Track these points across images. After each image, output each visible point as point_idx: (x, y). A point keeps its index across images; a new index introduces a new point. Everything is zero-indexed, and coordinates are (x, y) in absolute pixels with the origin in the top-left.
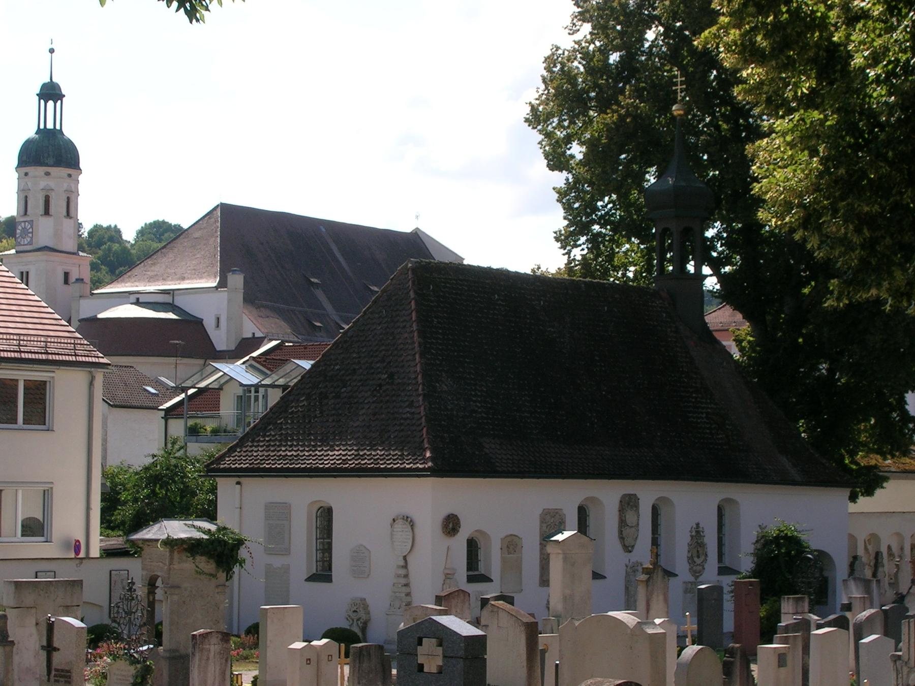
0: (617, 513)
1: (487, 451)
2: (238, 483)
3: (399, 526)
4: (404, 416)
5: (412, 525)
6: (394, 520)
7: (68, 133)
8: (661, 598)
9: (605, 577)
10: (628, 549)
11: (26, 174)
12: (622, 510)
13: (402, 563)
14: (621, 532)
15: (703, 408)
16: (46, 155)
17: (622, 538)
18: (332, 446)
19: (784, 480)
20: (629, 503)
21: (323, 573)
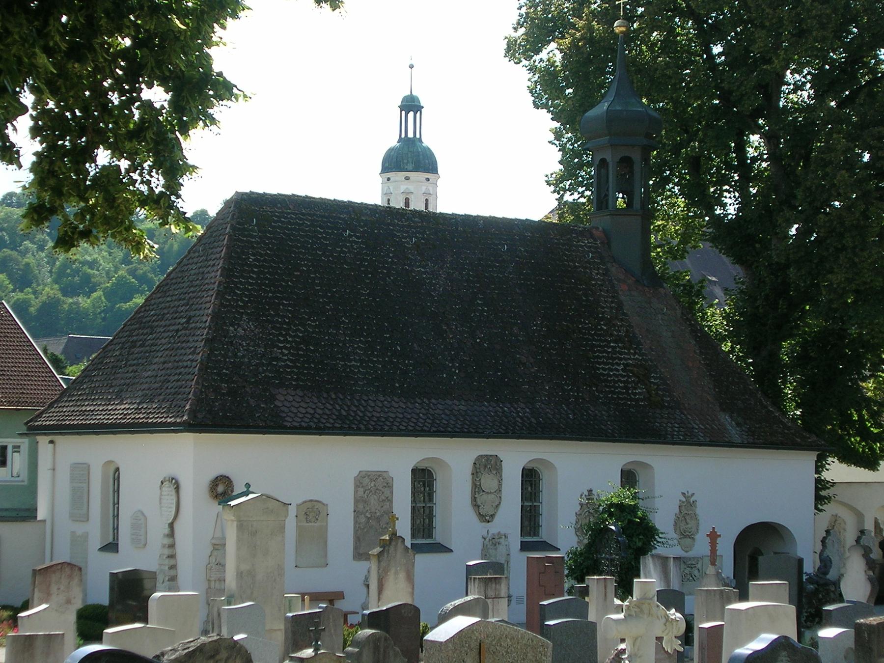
0: (469, 478)
1: (279, 404)
2: (51, 442)
3: (168, 489)
4: (185, 364)
5: (177, 489)
6: (162, 483)
7: (427, 141)
8: (402, 575)
9: (451, 551)
10: (486, 518)
11: (389, 179)
12: (475, 473)
13: (167, 531)
14: (474, 499)
15: (621, 359)
16: (405, 161)
17: (476, 505)
18: (122, 400)
19: (716, 440)
20: (488, 465)
21: (112, 547)
